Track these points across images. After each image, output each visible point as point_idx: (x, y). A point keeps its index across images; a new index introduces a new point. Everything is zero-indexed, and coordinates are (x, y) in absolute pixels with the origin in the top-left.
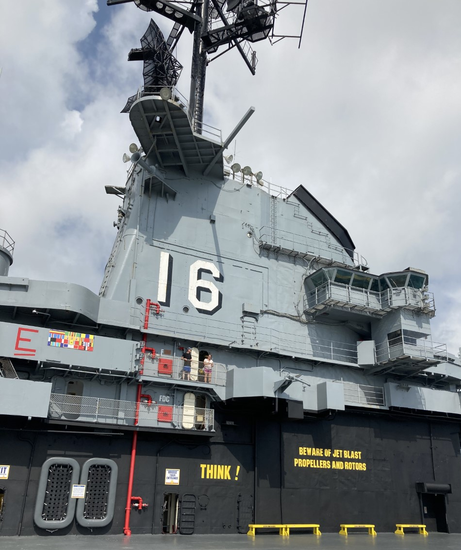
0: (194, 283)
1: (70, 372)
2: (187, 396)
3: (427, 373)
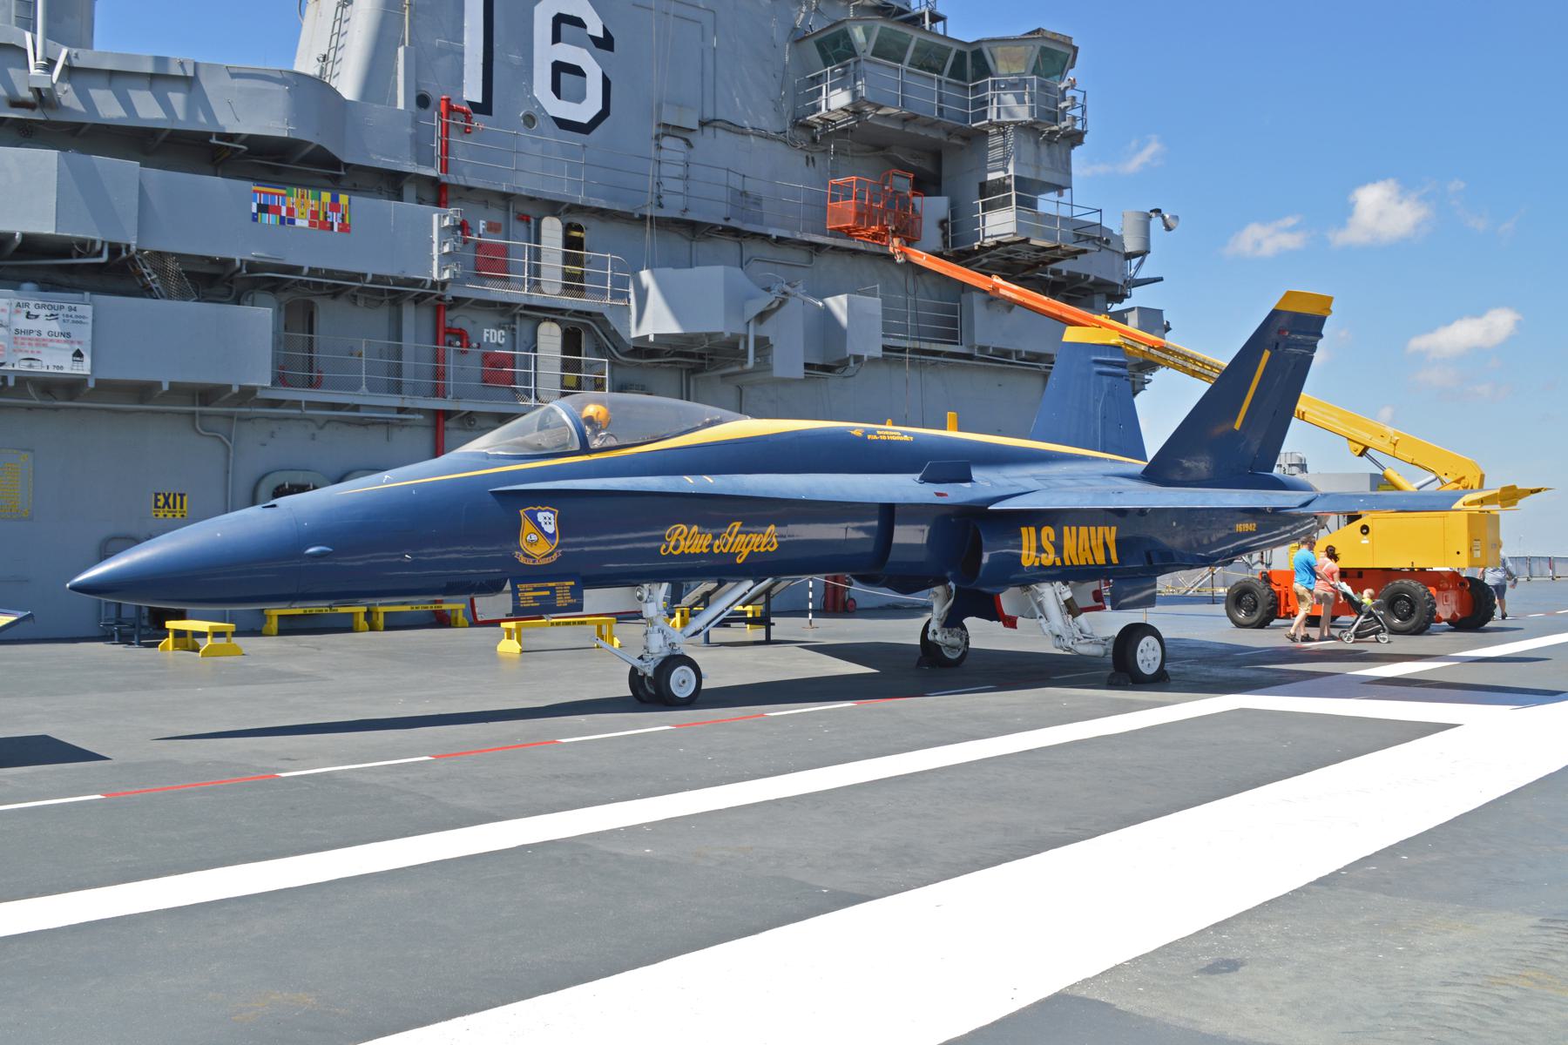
3: (1053, 272)
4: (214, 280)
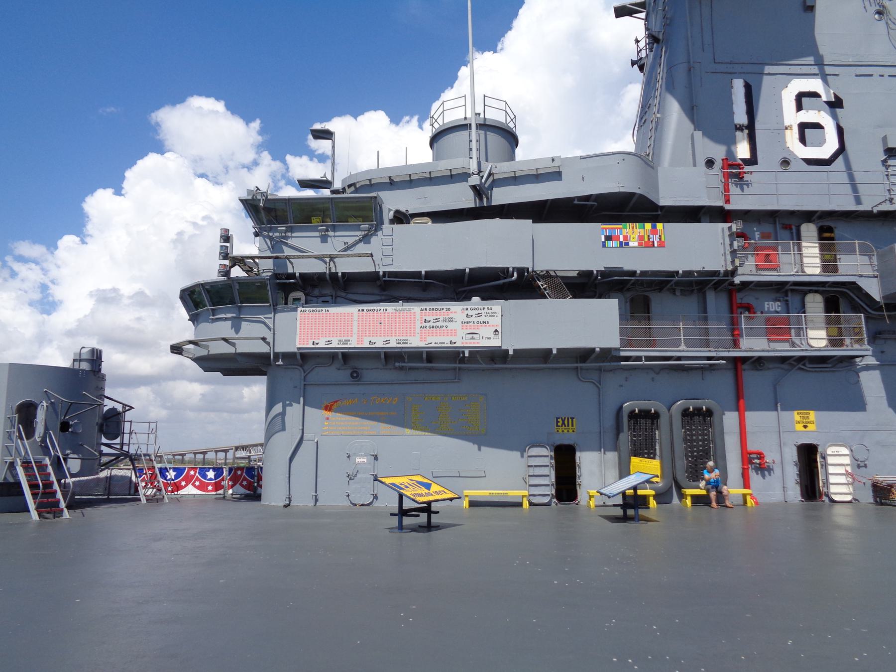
0: (792, 117)
2: (809, 298)
4: (584, 285)
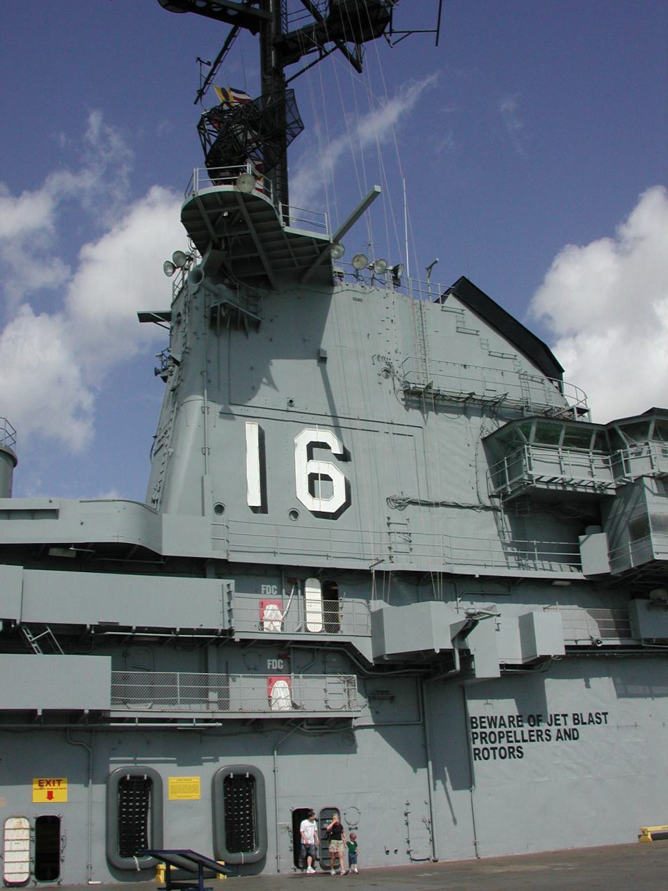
0: (303, 468)
1: (178, 639)
4: (74, 639)
